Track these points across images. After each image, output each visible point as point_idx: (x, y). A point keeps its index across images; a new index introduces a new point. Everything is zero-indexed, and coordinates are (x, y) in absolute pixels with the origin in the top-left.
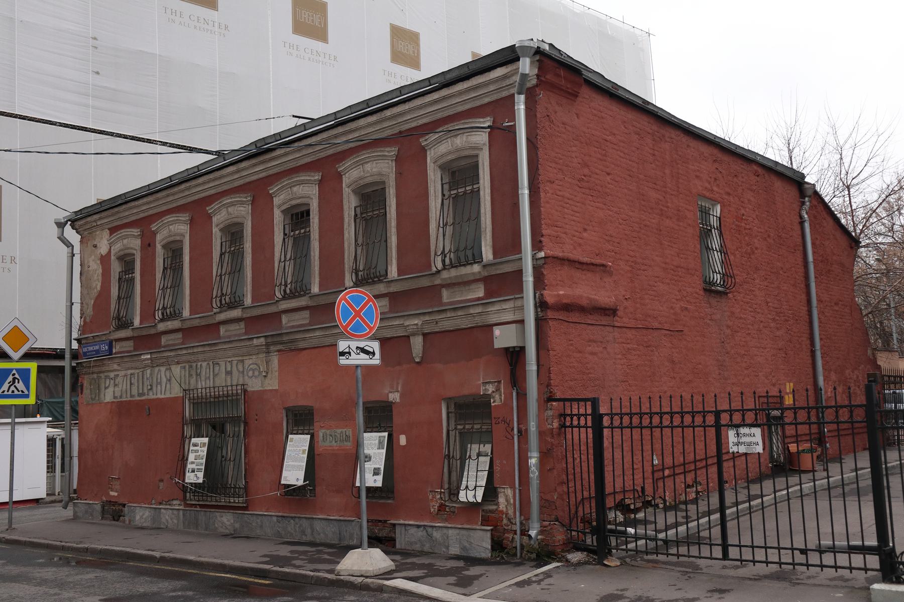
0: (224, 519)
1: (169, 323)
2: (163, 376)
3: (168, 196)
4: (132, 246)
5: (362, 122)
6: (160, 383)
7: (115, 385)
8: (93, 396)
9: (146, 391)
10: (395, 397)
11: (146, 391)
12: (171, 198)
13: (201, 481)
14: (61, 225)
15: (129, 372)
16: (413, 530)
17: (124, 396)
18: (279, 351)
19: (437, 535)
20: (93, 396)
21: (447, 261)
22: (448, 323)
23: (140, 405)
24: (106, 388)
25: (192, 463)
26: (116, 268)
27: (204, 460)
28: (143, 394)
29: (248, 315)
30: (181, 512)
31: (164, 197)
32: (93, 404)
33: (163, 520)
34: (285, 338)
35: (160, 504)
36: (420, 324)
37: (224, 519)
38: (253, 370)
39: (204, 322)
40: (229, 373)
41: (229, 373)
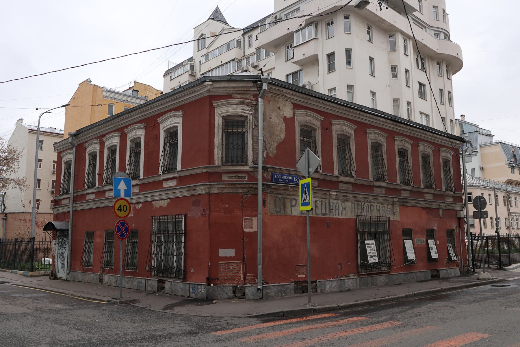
0: (381, 279)
1: (348, 178)
2: (340, 206)
6: (338, 209)
9: (327, 212)
10: (435, 228)
12: (347, 113)
13: (377, 261)
16: (444, 271)
18: (400, 205)
19: (449, 271)
25: (370, 253)
28: (327, 214)
30: (358, 279)
32: (277, 216)
33: (347, 285)
34: (405, 201)
35: (342, 277)
37: (381, 279)
38: (389, 211)
40: (378, 211)
41: (378, 211)
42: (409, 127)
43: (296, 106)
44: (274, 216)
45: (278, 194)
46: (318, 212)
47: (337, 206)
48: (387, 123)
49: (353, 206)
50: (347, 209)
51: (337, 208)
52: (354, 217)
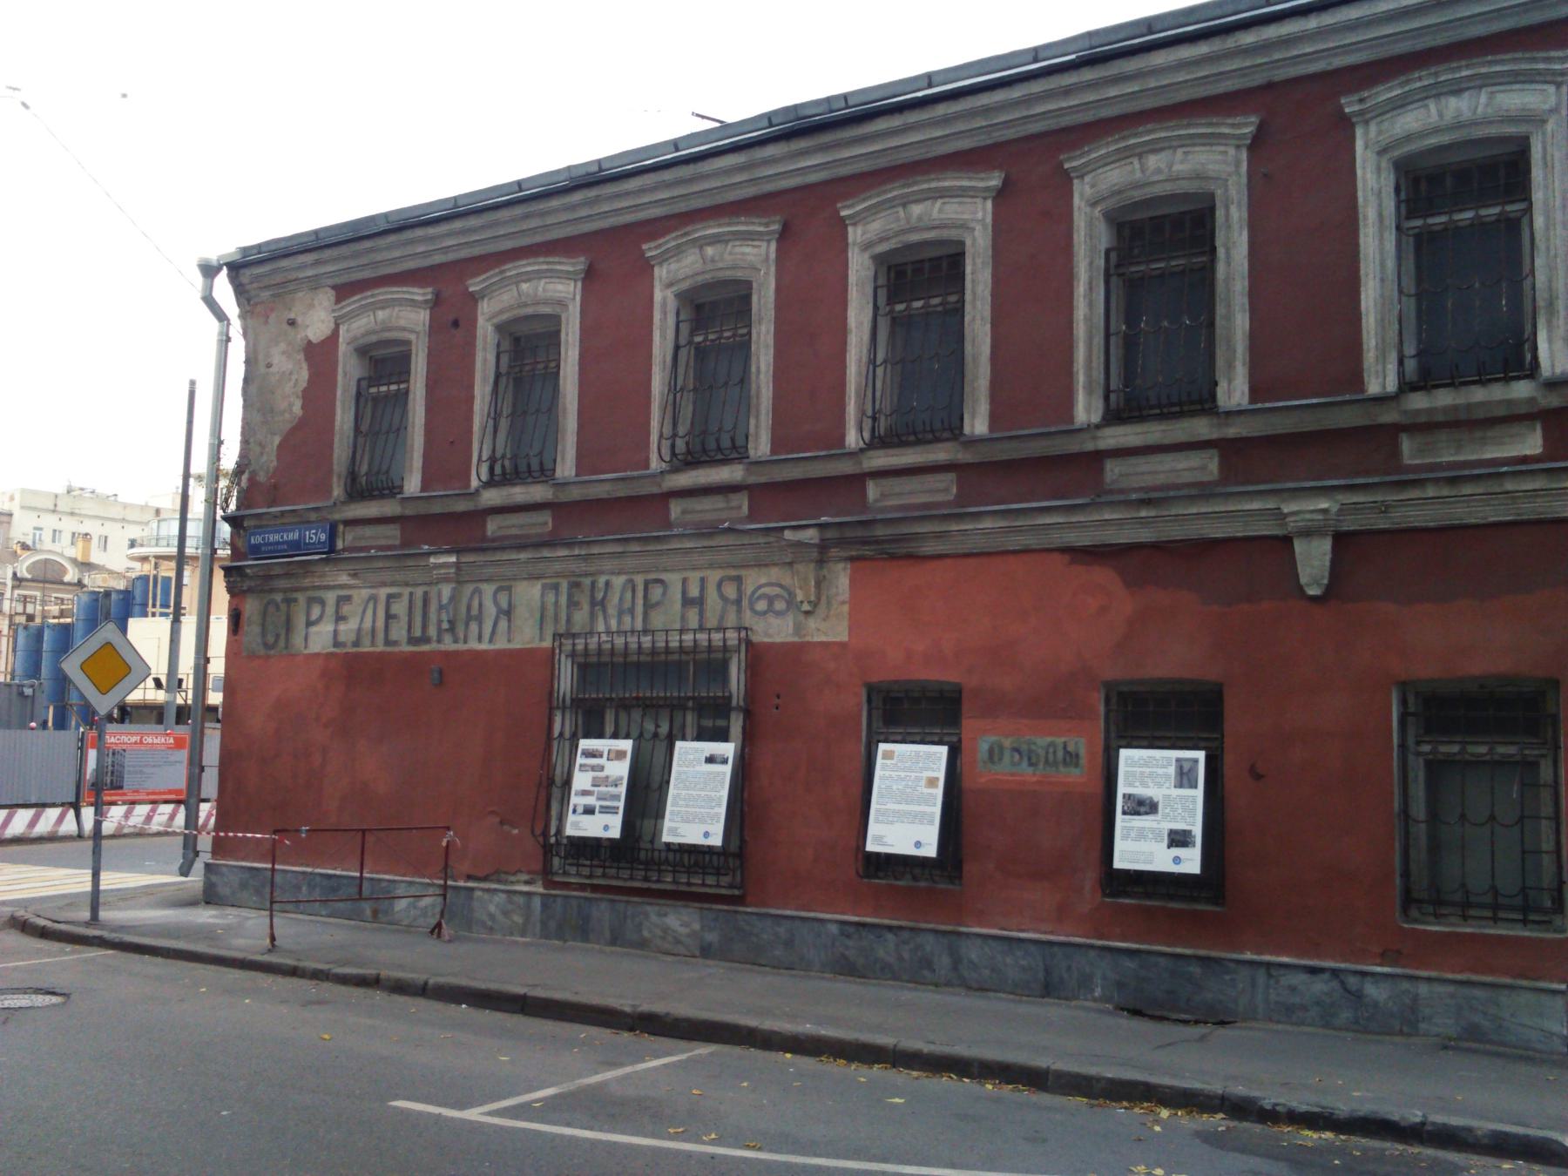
3: (526, 217)
4: (402, 323)
5: (1159, 58)
6: (479, 619)
7: (340, 618)
8: (271, 639)
11: (432, 632)
12: (533, 223)
14: (209, 271)
15: (383, 592)
17: (366, 641)
18: (852, 559)
20: (271, 639)
21: (498, 470)
22: (1419, 509)
23: (412, 666)
24: (309, 624)
25: (585, 793)
26: (348, 370)
27: (622, 790)
28: (425, 639)
29: (763, 480)
30: (537, 902)
31: (513, 220)
34: (880, 531)
36: (1335, 508)
38: (771, 600)
39: (622, 491)
42: (941, 110)
43: (343, 291)
44: (259, 657)
45: (272, 591)
46: (394, 636)
47: (476, 603)
48: (766, 162)
49: (551, 598)
50: (521, 612)
51: (627, 605)
52: (547, 644)
